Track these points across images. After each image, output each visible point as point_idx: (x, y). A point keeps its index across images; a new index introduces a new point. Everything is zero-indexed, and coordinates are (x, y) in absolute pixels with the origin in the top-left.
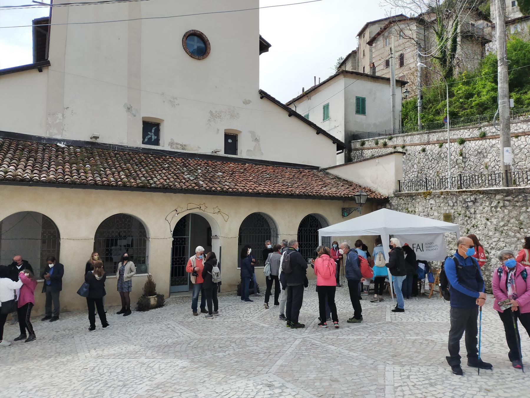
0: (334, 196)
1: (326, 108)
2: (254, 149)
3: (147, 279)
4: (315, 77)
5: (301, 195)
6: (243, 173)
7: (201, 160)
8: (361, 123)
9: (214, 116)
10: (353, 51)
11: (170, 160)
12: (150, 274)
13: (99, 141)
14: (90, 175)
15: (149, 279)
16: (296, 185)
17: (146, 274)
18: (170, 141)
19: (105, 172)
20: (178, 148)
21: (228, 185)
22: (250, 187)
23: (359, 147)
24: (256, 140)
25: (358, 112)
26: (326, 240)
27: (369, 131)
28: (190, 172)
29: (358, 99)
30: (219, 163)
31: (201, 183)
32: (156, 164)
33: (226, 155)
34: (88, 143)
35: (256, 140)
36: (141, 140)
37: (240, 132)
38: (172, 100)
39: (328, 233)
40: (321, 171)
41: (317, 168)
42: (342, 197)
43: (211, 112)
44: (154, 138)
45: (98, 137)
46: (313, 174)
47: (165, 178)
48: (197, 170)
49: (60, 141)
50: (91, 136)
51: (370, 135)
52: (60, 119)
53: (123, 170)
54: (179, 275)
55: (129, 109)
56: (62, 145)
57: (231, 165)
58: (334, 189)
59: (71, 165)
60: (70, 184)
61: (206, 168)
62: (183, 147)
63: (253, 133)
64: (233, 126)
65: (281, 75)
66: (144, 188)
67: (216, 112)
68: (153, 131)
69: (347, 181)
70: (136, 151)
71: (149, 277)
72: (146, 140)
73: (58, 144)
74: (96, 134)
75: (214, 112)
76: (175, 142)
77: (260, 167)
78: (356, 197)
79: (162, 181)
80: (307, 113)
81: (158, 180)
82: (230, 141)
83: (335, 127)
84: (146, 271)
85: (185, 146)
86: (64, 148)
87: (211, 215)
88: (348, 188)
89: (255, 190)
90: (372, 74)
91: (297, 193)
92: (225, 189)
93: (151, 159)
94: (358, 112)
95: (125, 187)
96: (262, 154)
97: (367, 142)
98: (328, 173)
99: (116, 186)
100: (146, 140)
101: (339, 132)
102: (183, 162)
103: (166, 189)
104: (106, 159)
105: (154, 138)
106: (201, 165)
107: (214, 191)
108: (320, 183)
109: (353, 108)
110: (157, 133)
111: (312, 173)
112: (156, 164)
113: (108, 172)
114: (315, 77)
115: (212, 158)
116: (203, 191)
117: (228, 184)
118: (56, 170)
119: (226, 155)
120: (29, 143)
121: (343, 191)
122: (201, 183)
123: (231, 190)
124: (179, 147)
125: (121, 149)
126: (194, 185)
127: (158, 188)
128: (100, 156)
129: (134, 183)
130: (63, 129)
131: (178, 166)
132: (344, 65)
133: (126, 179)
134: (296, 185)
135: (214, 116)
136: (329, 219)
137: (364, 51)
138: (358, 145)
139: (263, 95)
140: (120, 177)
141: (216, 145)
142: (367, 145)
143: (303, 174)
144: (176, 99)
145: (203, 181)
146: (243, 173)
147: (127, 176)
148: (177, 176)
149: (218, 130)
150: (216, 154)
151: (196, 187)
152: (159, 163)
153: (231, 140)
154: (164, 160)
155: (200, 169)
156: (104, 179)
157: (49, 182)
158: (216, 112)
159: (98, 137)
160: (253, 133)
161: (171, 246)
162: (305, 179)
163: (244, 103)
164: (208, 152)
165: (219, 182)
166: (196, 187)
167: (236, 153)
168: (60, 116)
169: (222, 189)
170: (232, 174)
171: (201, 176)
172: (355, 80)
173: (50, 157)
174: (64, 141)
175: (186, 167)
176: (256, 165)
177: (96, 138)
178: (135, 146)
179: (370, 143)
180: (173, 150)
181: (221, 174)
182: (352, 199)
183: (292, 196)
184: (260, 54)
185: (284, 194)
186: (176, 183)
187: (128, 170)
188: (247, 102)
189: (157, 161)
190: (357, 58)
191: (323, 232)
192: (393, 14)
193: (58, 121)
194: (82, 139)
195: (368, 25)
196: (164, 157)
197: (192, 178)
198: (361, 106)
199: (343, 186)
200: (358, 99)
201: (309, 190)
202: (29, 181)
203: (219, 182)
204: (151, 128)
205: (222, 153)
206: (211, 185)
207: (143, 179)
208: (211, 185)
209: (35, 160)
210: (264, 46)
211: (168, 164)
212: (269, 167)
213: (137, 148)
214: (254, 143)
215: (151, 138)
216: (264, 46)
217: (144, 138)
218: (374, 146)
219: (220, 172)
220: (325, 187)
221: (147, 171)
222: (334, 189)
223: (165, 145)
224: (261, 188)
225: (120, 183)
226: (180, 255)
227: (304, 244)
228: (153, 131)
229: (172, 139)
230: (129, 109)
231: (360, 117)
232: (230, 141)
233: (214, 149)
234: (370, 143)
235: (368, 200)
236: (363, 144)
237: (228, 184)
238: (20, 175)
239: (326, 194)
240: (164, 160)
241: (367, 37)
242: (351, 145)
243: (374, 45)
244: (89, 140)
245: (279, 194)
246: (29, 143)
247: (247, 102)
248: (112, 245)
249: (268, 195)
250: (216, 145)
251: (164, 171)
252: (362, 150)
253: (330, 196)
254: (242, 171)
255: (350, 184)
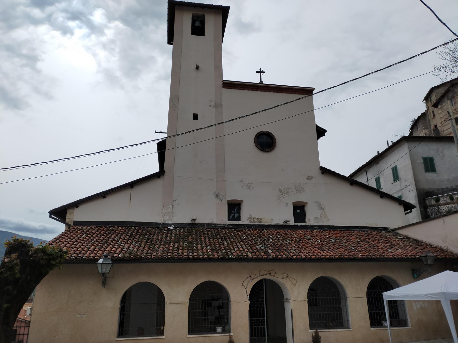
0: (399, 258)
1: (395, 170)
2: (321, 217)
3: (228, 339)
4: (387, 141)
5: (364, 259)
6: (310, 239)
7: (274, 230)
8: (431, 181)
9: (283, 192)
10: (422, 114)
11: (249, 232)
12: (232, 334)
13: (197, 222)
14: (185, 251)
15: (230, 338)
16: (360, 249)
17: (228, 334)
18: (248, 216)
19: (197, 247)
20: (255, 222)
21: (292, 252)
22: (314, 252)
23: (435, 203)
24: (322, 208)
25: (427, 171)
26: (393, 304)
27: (444, 187)
28: (263, 242)
29: (425, 159)
30: (289, 231)
31: (270, 251)
32: (236, 237)
33: (296, 224)
34: (189, 224)
35: (322, 208)
36: (227, 217)
37: (307, 203)
38: (249, 184)
39: (391, 297)
40: (390, 232)
41: (386, 229)
42: (408, 258)
43: (280, 190)
44: (237, 215)
45: (196, 220)
46: (381, 235)
47: (241, 249)
48: (269, 240)
49: (170, 225)
50: (191, 219)
51: (443, 191)
52: (171, 209)
53: (210, 245)
54: (258, 336)
55: (217, 195)
56: (171, 228)
57: (301, 232)
58: (400, 251)
59: (174, 243)
60: (171, 259)
61: (277, 237)
62: (259, 220)
63: (318, 203)
64: (300, 198)
65: (341, 153)
66: (223, 259)
67: (284, 189)
68: (236, 210)
69: (417, 240)
70: (223, 227)
71: (230, 337)
72: (231, 217)
73: (169, 227)
74: (194, 217)
75: (282, 190)
76: (253, 216)
77: (327, 232)
78: (423, 258)
79: (238, 252)
80: (378, 176)
81: (235, 252)
82: (298, 211)
83: (406, 187)
84: (229, 332)
85: (261, 219)
86: (173, 230)
87: (281, 280)
88: (416, 248)
89: (317, 256)
90: (435, 135)
91: (360, 256)
92: (289, 257)
93: (234, 233)
94: (427, 171)
95: (209, 260)
96: (329, 220)
97: (441, 199)
98: (397, 234)
99: (202, 259)
100: (231, 217)
101: (411, 191)
102: (259, 233)
103: (240, 259)
104: (200, 236)
105: (237, 215)
106: (273, 234)
107: (280, 259)
108: (386, 245)
109: (421, 168)
110: (239, 211)
111: (380, 234)
112: (236, 237)
113: (199, 248)
114: (387, 141)
115: (285, 227)
116: (271, 259)
117: (293, 251)
118: (164, 249)
119: (296, 224)
120: (150, 229)
121: (410, 252)
122: (270, 251)
123: (295, 257)
124: (256, 220)
125: (212, 226)
126: (263, 254)
127: (233, 259)
128: (196, 234)
129: (215, 256)
130: (173, 216)
131: (254, 238)
132: (416, 127)
133: (210, 253)
134: (360, 249)
135: (283, 192)
136: (399, 281)
137: (433, 112)
138: (433, 202)
139: (324, 171)
140: (207, 251)
141: (286, 216)
142: (442, 201)
143: (371, 236)
144: (252, 183)
145: (272, 250)
146: (310, 239)
147: (212, 250)
148: (251, 247)
149: (287, 204)
150: (287, 224)
151: (265, 256)
152: (239, 236)
153: (299, 210)
154: (244, 233)
155: (272, 239)
156: (195, 254)
157: (157, 259)
158: (284, 189)
159: (196, 220)
160: (318, 203)
161: (248, 309)
162: (371, 242)
163: (307, 179)
164: (280, 222)
165: (285, 250)
166: (265, 256)
167: (304, 221)
168: (171, 206)
169: (287, 256)
170: (299, 241)
171: (271, 246)
172: (418, 143)
173: (162, 239)
174: (173, 224)
175: (260, 238)
176: (324, 231)
177: (195, 220)
178: (222, 223)
179: (445, 199)
180: (251, 224)
181: (289, 242)
182: (420, 259)
183: (354, 260)
184: (318, 139)
185: (346, 258)
186: (249, 254)
187: (214, 244)
188: (309, 178)
189: (238, 234)
190: (427, 119)
191: (389, 295)
192: (449, 79)
193: (169, 210)
194: (185, 222)
195: (432, 90)
196: (244, 230)
197: (262, 248)
198: (429, 165)
199: (411, 246)
200: (425, 159)
201: (374, 253)
202: (144, 260)
203: (285, 250)
204: (234, 208)
205: (292, 222)
206: (278, 254)
207: (224, 251)
208: (278, 254)
209: (152, 242)
210: (321, 132)
211: (246, 236)
212: (336, 232)
213: (224, 224)
214: (320, 212)
215: (234, 215)
216: (321, 132)
217: (229, 216)
218: (449, 201)
219: (289, 240)
220: (391, 249)
221: (228, 245)
222: (400, 251)
223: (245, 221)
224: (323, 254)
225: (206, 256)
226: (257, 317)
227: (376, 307)
228: (236, 210)
229: (250, 215)
230: (217, 196)
231: (431, 176)
232: (298, 211)
233: (285, 219)
234: (445, 199)
235: (436, 260)
236: (437, 200)
237: (293, 251)
238: (139, 256)
239: (391, 256)
240: (244, 233)
241: (434, 98)
242: (425, 202)
243: (439, 107)
244: (189, 222)
245: (342, 259)
246: (150, 229)
247: (309, 178)
248: (208, 307)
249: (330, 260)
250: (286, 216)
251: (242, 243)
252: (438, 206)
253: (395, 258)
254: (309, 237)
255: (419, 243)
